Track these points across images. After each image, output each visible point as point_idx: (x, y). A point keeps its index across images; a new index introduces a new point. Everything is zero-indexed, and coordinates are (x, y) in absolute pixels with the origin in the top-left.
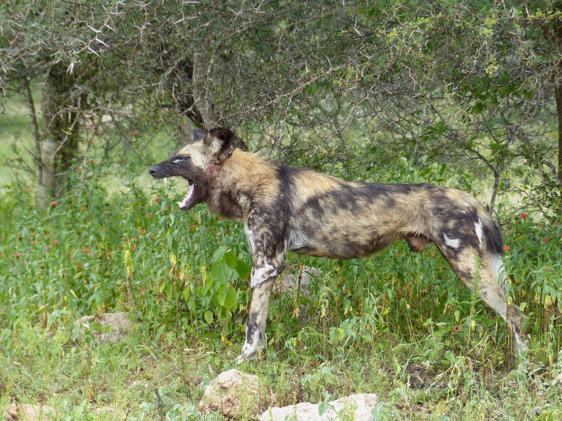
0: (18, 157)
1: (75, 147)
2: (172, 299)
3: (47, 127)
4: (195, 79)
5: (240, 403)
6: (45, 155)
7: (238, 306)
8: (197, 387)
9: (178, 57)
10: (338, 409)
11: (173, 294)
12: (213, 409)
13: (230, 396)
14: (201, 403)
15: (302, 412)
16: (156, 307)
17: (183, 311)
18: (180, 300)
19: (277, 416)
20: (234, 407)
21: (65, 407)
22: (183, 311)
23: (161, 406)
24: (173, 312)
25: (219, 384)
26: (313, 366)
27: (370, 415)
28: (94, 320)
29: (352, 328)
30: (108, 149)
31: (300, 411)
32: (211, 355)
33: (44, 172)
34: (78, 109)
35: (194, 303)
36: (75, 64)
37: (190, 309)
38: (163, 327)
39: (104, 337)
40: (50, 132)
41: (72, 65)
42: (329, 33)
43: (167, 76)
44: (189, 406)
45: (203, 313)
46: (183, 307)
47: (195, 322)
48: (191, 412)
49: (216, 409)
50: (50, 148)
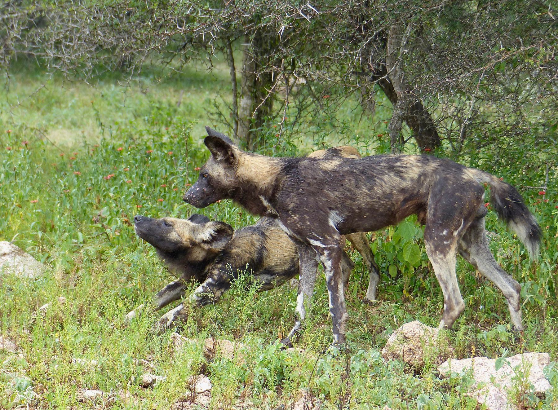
0: (218, 111)
1: (271, 106)
4: (390, 50)
5: (420, 353)
6: (242, 110)
7: (421, 262)
9: (378, 28)
10: (513, 365)
12: (395, 356)
13: (411, 346)
14: (384, 351)
15: (478, 365)
19: (455, 368)
20: (414, 356)
21: (258, 345)
25: (402, 334)
26: (487, 323)
27: (542, 373)
29: (527, 291)
30: (301, 109)
31: (477, 365)
34: (281, 70)
39: (292, 282)
40: (247, 90)
42: (521, 15)
44: (374, 352)
45: (388, 267)
49: (398, 357)
50: (247, 104)
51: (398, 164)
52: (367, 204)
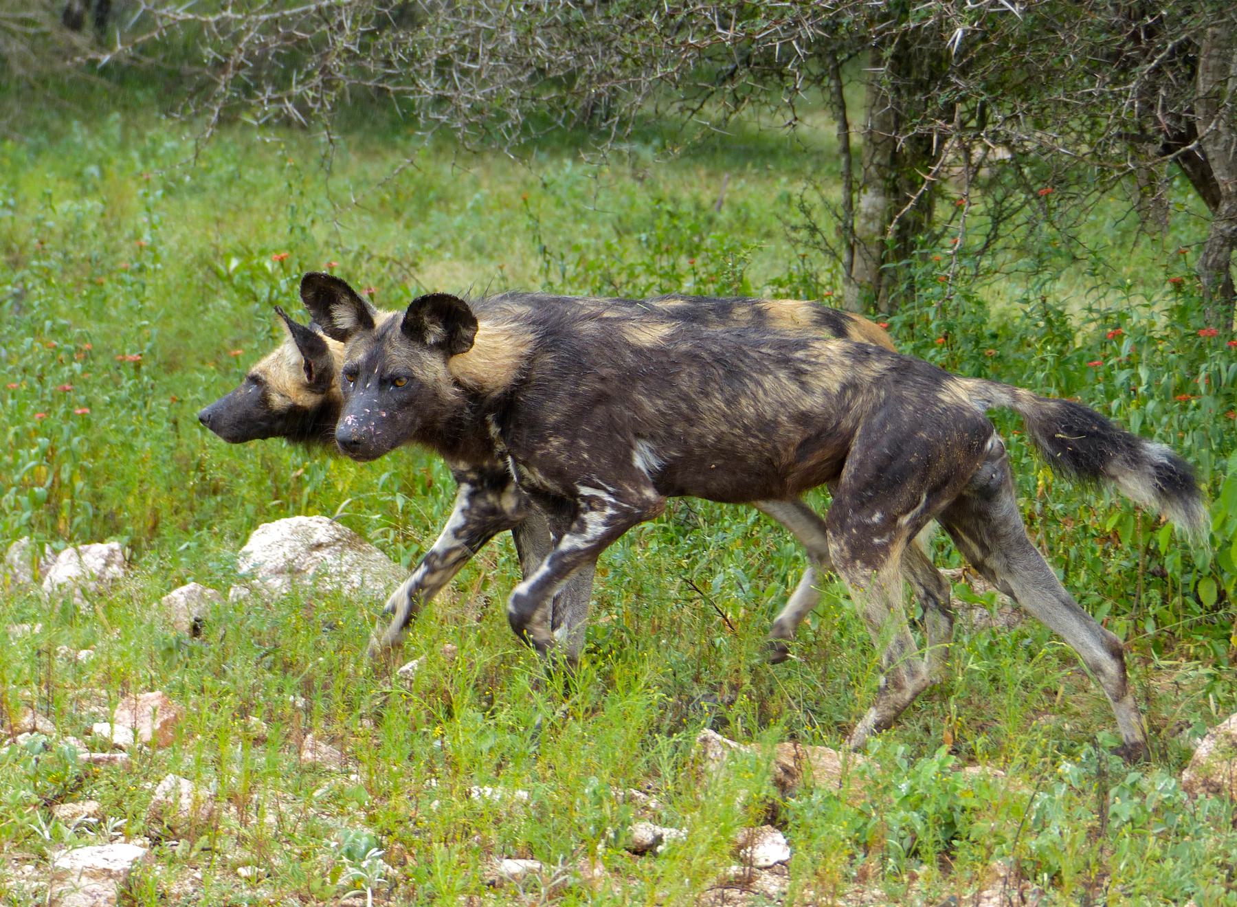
2: (1132, 547)
3: (871, 163)
4: (1204, 84)
6: (863, 221)
8: (1175, 739)
11: (1134, 537)
12: (1212, 788)
14: (1186, 775)
16: (1096, 561)
17: (1154, 574)
18: (1147, 550)
22: (1154, 574)
23: (1101, 774)
24: (1129, 576)
28: (960, 578)
32: (1209, 675)
33: (856, 258)
35: (1178, 560)
36: (965, 32)
37: (1169, 571)
38: (1107, 606)
39: (977, 616)
40: (875, 174)
41: (959, 33)
43: (1149, 73)
45: (1197, 583)
46: (1154, 566)
47: (1177, 600)
48: (1167, 792)
49: (1218, 790)
50: (874, 207)
51: (800, 354)
52: (719, 438)
